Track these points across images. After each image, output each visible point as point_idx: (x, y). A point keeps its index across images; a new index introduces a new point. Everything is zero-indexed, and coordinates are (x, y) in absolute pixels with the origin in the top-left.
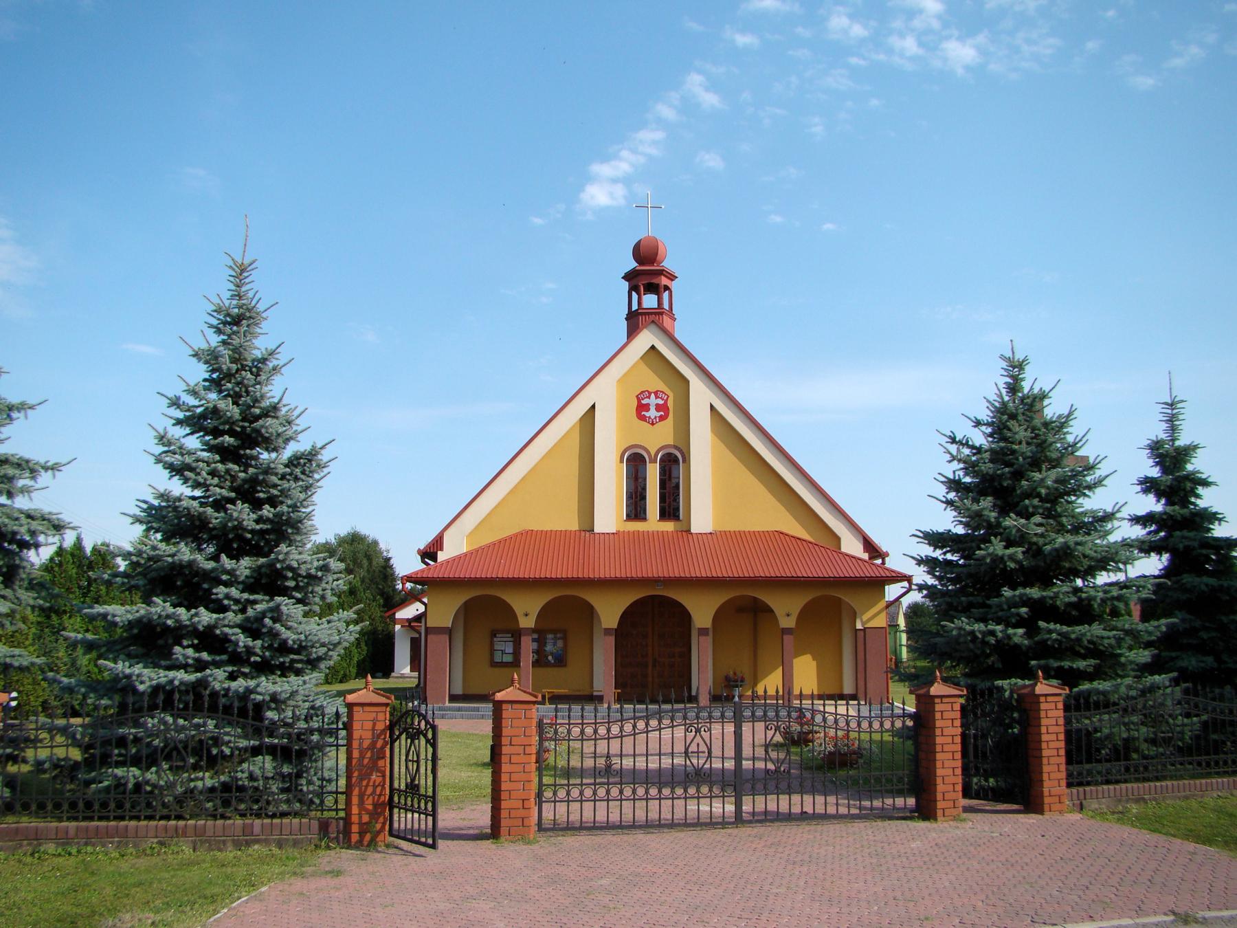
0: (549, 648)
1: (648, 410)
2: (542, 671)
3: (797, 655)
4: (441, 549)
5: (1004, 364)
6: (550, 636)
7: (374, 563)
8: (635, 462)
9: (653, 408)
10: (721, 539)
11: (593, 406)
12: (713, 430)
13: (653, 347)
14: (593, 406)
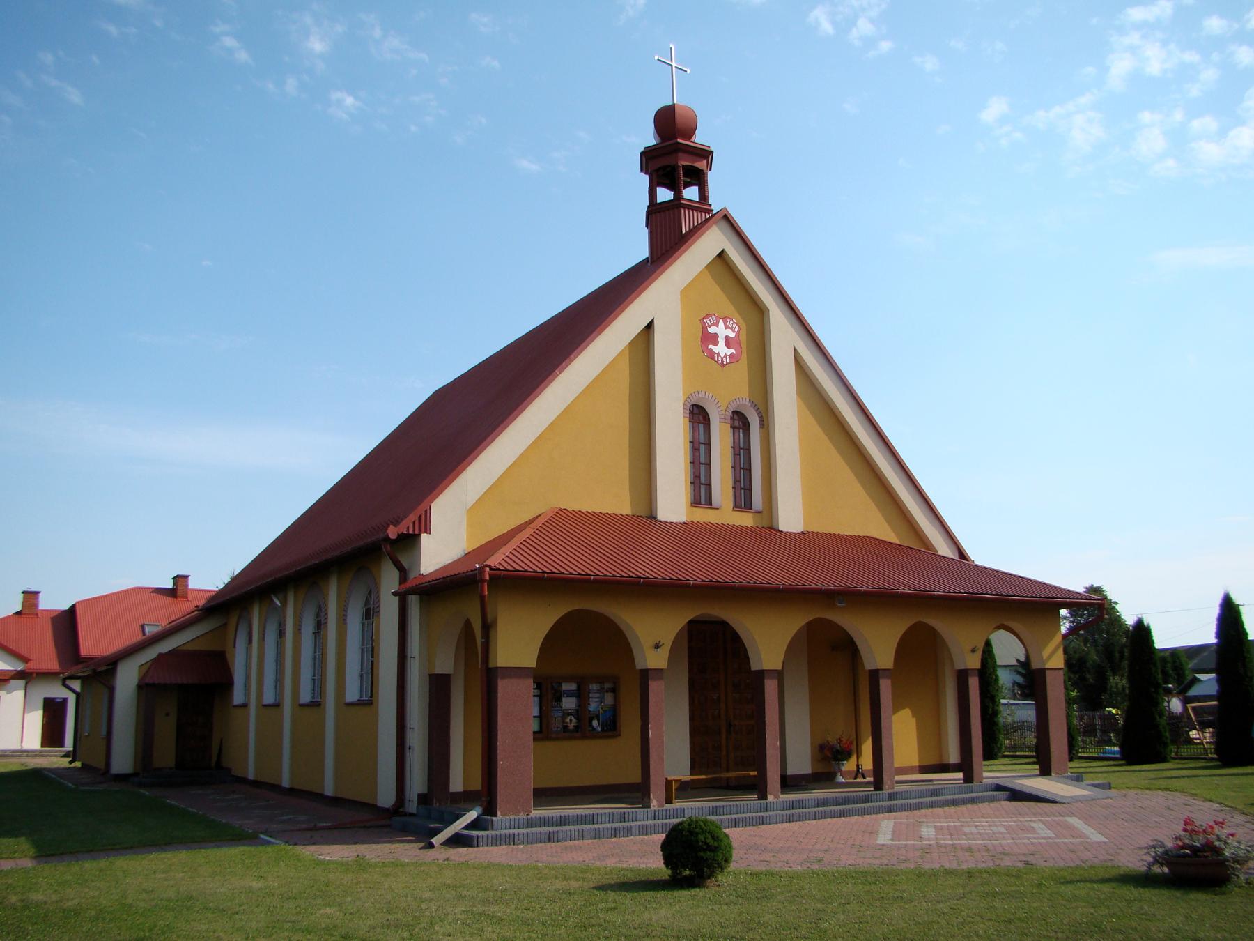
0: (593, 706)
1: (716, 344)
2: (550, 745)
3: (896, 708)
4: (427, 531)
5: (1023, 659)
6: (594, 687)
7: (412, 575)
8: (698, 415)
9: (722, 341)
10: (806, 541)
11: (650, 326)
12: (799, 393)
13: (722, 255)
14: (650, 326)
